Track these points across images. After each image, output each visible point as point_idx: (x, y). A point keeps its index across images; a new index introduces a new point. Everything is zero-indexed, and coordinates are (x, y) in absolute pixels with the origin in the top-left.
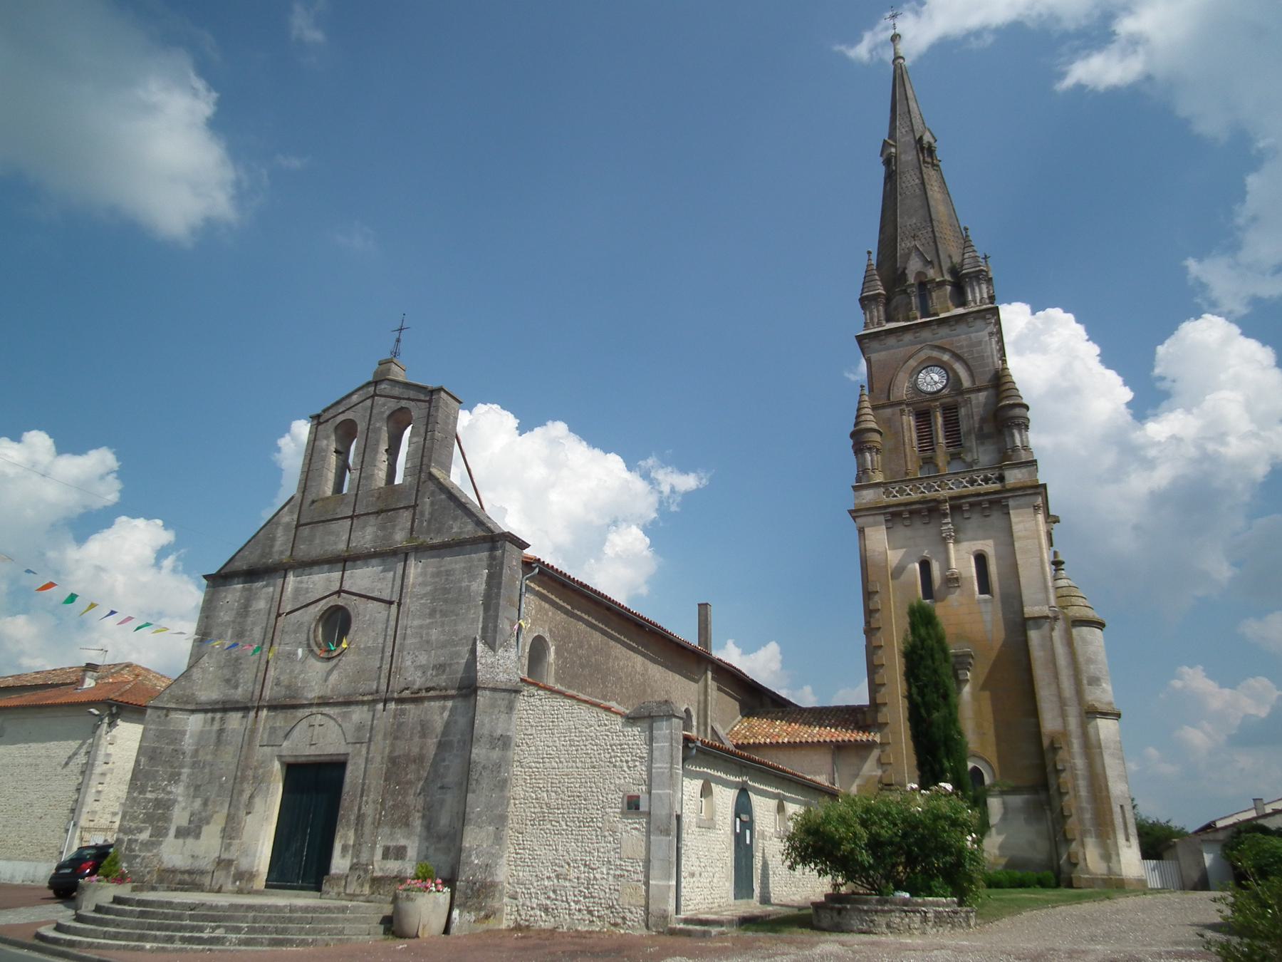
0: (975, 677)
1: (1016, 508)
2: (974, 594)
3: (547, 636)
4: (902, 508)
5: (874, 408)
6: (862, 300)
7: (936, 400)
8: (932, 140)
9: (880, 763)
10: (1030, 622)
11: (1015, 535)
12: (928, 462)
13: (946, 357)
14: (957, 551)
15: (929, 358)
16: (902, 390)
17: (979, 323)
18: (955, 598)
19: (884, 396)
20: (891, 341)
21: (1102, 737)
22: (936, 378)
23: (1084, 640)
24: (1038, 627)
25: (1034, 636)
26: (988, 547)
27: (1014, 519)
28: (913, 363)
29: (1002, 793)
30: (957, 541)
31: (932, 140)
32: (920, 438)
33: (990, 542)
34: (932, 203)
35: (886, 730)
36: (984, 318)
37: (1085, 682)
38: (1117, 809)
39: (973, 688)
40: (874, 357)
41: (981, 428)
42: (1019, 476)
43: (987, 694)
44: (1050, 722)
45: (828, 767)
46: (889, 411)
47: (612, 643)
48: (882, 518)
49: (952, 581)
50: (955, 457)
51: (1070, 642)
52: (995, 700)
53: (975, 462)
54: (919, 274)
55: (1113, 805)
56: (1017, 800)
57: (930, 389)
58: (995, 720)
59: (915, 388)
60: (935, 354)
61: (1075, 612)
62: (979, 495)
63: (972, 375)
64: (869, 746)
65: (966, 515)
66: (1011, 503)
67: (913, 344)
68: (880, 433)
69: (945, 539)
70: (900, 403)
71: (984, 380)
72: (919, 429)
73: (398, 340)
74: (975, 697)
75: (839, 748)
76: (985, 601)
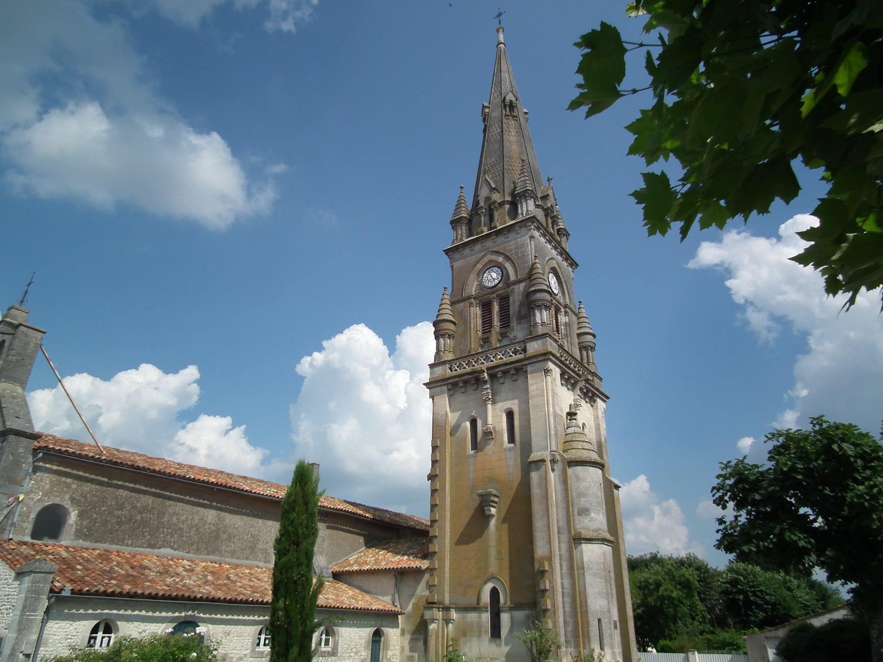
0: (498, 512)
1: (533, 372)
2: (464, 447)
3: (67, 504)
4: (457, 379)
5: (452, 304)
6: (452, 222)
7: (493, 293)
8: (514, 99)
9: (430, 587)
10: (533, 465)
11: (530, 394)
12: (486, 341)
13: (500, 259)
14: (494, 410)
15: (491, 261)
16: (473, 289)
17: (524, 230)
18: (490, 448)
19: (459, 293)
20: (467, 251)
21: (585, 559)
22: (494, 275)
23: (578, 478)
24: (538, 469)
25: (534, 475)
26: (514, 405)
27: (530, 381)
28: (479, 266)
29: (511, 609)
30: (494, 402)
31: (514, 99)
32: (484, 323)
33: (516, 402)
34: (506, 144)
35: (436, 557)
36: (526, 226)
37: (576, 512)
38: (594, 623)
39: (497, 521)
40: (456, 264)
41: (519, 311)
42: (536, 347)
43: (506, 526)
44: (540, 550)
45: (392, 589)
46: (462, 305)
47: (168, 503)
48: (445, 388)
49: (488, 434)
50: (503, 335)
51: (565, 480)
52: (511, 530)
53: (515, 337)
54: (488, 199)
55: (590, 618)
56: (520, 614)
57: (490, 285)
58: (510, 547)
59: (481, 286)
60: (494, 257)
61: (573, 455)
62: (506, 364)
63: (516, 271)
64: (418, 573)
65: (501, 381)
66: (529, 368)
67: (481, 251)
68: (454, 323)
69: (485, 401)
70: (469, 298)
71: (523, 274)
72: (483, 317)
73: (26, 292)
74: (498, 529)
75: (401, 574)
76: (510, 449)
